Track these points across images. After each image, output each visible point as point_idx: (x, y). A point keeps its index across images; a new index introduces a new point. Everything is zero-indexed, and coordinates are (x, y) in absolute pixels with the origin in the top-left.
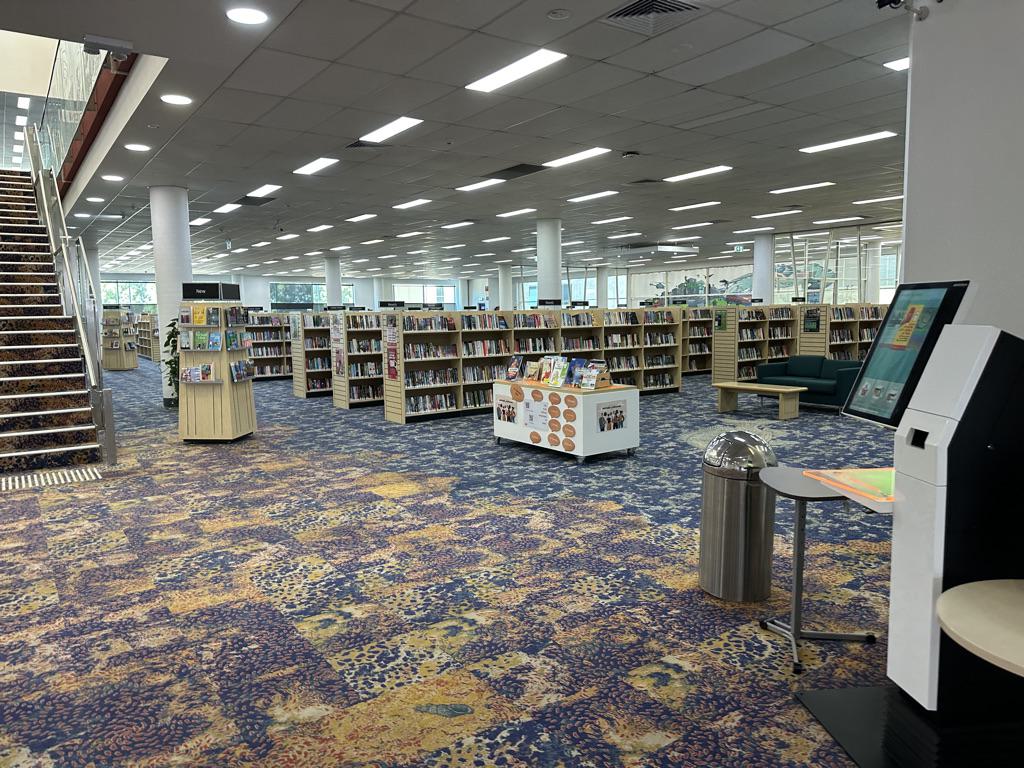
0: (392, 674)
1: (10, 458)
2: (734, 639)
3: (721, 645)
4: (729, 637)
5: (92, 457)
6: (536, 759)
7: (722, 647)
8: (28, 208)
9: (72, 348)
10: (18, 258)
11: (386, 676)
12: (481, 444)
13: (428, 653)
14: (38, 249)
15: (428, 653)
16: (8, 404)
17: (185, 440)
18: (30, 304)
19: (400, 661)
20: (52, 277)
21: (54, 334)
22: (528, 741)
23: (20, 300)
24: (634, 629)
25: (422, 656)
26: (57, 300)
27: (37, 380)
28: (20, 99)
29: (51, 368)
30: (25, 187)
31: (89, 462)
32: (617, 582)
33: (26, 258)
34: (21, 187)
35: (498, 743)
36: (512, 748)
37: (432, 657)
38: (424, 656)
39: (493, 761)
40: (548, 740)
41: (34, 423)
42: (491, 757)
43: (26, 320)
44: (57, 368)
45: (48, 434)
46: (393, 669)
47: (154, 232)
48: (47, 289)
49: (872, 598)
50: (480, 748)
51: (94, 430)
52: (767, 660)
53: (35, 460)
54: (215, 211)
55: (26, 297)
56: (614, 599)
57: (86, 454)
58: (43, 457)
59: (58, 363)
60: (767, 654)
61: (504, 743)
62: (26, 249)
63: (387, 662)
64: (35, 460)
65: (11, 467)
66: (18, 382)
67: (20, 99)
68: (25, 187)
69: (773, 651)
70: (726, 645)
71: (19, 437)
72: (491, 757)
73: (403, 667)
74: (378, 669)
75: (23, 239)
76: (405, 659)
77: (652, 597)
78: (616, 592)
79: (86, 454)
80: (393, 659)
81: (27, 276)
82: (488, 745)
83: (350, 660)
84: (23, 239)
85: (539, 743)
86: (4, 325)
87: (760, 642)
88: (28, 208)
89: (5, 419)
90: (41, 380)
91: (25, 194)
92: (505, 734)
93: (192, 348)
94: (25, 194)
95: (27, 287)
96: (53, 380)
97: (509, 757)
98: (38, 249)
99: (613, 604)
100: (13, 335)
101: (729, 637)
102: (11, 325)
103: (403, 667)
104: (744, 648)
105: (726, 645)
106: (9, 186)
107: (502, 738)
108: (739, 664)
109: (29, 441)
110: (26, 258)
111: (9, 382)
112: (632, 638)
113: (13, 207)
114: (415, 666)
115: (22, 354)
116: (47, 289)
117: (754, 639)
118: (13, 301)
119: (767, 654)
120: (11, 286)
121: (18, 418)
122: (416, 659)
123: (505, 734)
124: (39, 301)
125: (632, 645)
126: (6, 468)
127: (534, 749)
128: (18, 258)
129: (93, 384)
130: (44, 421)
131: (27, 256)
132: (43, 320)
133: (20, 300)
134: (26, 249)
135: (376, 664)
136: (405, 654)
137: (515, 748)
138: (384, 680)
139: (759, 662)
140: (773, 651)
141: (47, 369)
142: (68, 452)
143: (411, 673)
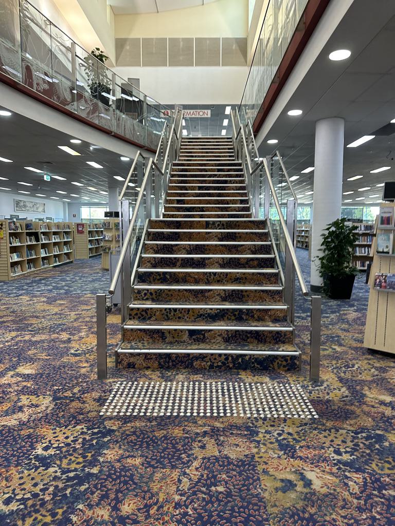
0: (317, 392)
1: (220, 355)
5: (292, 365)
6: (376, 451)
8: (230, 156)
9: (266, 245)
10: (226, 182)
11: (313, 392)
13: (338, 388)
14: (237, 176)
15: (338, 388)
16: (219, 295)
17: (369, 349)
18: (232, 211)
19: (322, 387)
20: (246, 193)
21: (252, 233)
22: (376, 442)
23: (226, 209)
25: (334, 389)
26: (248, 209)
27: (241, 273)
28: (227, 107)
29: (251, 262)
30: (229, 145)
31: (289, 370)
33: (230, 182)
34: (227, 145)
35: (358, 437)
36: (365, 442)
37: (340, 390)
38: (335, 389)
39: (352, 444)
40: (388, 445)
41: (239, 316)
42: (352, 441)
43: (233, 221)
44: (256, 263)
45: (251, 332)
46: (318, 390)
48: (242, 202)
50: (347, 436)
51: (292, 332)
53: (240, 360)
55: (230, 207)
57: (286, 361)
58: (247, 358)
59: (257, 259)
61: (361, 439)
62: (230, 176)
63: (316, 386)
64: (240, 360)
65: (220, 364)
66: (227, 274)
67: (227, 107)
68: (229, 145)
71: (227, 331)
72: (352, 441)
73: (323, 391)
74: (310, 388)
75: (229, 170)
76: (325, 388)
79: (286, 361)
80: (319, 386)
81: (231, 193)
82: (352, 436)
83: (298, 381)
84: (229, 170)
85: (382, 445)
86: (218, 225)
88: (230, 156)
89: (217, 309)
90: (244, 274)
91: (229, 149)
92: (364, 435)
93: (391, 252)
94: (229, 149)
95: (231, 200)
96: (253, 274)
97: (362, 445)
98: (237, 176)
100: (224, 233)
102: (223, 225)
103: (323, 391)
106: (221, 145)
107: (362, 436)
109: (235, 336)
110: (230, 182)
111: (221, 273)
113: (223, 156)
114: (329, 392)
115: (230, 249)
116: (242, 202)
118: (222, 209)
120: (221, 200)
121: (228, 309)
122: (331, 389)
123: (364, 435)
124: (237, 210)
126: (215, 365)
127: (377, 446)
128: (226, 182)
129: (304, 291)
130: (247, 314)
131: (231, 181)
132: (245, 221)
133: (226, 209)
134: (230, 176)
135: (310, 386)
136: (326, 386)
137: (367, 443)
138: (312, 393)
141: (247, 263)
142: (270, 356)
143: (326, 394)
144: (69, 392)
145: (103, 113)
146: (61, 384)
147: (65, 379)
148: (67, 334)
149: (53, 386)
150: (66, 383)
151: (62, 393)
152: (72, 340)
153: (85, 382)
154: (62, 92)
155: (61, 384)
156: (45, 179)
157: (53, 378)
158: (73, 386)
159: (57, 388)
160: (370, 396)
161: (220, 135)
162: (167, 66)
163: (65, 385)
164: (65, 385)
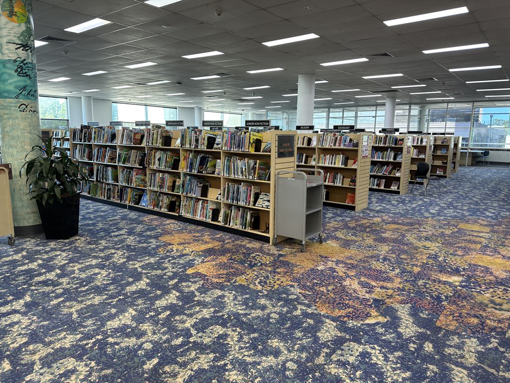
2: (272, 285)
3: (277, 282)
4: (274, 286)
7: (277, 281)
12: (99, 209)
24: (279, 274)
32: (254, 262)
47: (298, 106)
49: (364, 294)
52: (258, 278)
54: (146, 2)
56: (254, 255)
60: (258, 280)
69: (255, 282)
70: (275, 282)
77: (238, 257)
78: (254, 258)
87: (261, 285)
99: (253, 253)
101: (274, 286)
104: (268, 281)
105: (275, 282)
108: (269, 275)
112: (278, 270)
117: (263, 286)
119: (258, 280)
125: (278, 268)
139: (261, 277)
140: (255, 282)
144: (325, 288)
145: (9, 79)
146: (320, 279)
147: (325, 276)
148: (337, 273)
149: (314, 279)
150: (324, 279)
151: (319, 287)
152: (336, 262)
153: (340, 283)
154: (115, 62)
155: (320, 279)
156: (431, 345)
157: (315, 272)
158: (329, 284)
159: (316, 281)
160: (18, 315)
161: (436, 173)
162: (355, 189)
163: (323, 281)
164: (323, 281)
